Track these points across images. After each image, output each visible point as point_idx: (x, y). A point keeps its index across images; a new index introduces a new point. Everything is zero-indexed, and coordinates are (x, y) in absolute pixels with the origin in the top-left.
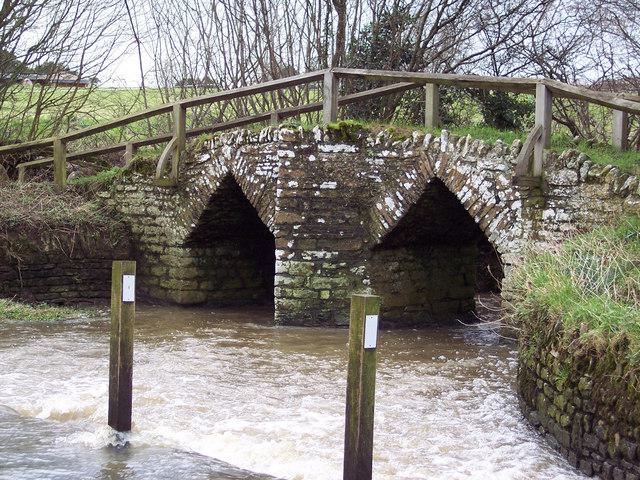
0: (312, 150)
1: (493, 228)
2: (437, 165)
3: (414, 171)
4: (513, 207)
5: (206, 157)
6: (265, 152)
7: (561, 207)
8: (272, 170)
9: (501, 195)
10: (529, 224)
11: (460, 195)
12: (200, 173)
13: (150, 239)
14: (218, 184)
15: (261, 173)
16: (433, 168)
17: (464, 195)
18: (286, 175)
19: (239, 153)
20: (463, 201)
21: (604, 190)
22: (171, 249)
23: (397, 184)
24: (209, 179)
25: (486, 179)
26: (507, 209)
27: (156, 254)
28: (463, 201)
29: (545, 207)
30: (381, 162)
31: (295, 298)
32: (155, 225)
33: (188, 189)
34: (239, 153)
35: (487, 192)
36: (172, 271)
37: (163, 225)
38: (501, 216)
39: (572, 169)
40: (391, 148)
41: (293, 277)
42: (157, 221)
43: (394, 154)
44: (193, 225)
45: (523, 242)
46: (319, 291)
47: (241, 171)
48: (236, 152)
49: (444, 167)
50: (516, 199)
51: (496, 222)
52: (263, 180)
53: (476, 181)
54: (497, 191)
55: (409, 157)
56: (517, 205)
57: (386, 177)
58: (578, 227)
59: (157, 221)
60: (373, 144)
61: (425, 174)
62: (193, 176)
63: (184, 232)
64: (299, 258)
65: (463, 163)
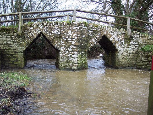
0: (81, 28)
1: (117, 46)
2: (105, 33)
3: (100, 34)
4: (122, 42)
5: (32, 28)
6: (55, 27)
7: (135, 42)
8: (58, 32)
9: (119, 39)
10: (126, 45)
11: (110, 39)
12: (31, 33)
13: (9, 51)
14: (37, 35)
15: (54, 33)
16: (104, 33)
17: (111, 39)
18: (78, 33)
19: (45, 27)
20: (111, 40)
21: (146, 39)
22: (18, 53)
23: (96, 36)
24: (35, 33)
25: (116, 36)
26: (121, 42)
27: (12, 55)
28: (111, 40)
29: (131, 42)
30: (92, 31)
31: (79, 63)
32: (11, 47)
33: (25, 37)
34: (45, 27)
35: (116, 39)
36: (19, 59)
37: (14, 46)
38: (119, 43)
39: (138, 34)
40: (95, 28)
41: (79, 58)
42: (12, 46)
43: (96, 30)
44: (27, 46)
45: (125, 49)
46: (82, 61)
47: (46, 32)
48: (44, 27)
49: (107, 33)
50: (123, 40)
51: (118, 45)
52: (54, 34)
53: (114, 36)
54: (118, 38)
55: (99, 31)
56: (123, 41)
57: (93, 35)
58: (139, 45)
59: (12, 46)
60: (90, 27)
61: (102, 34)
62: (27, 33)
63: (24, 49)
64: (79, 54)
65: (111, 32)
